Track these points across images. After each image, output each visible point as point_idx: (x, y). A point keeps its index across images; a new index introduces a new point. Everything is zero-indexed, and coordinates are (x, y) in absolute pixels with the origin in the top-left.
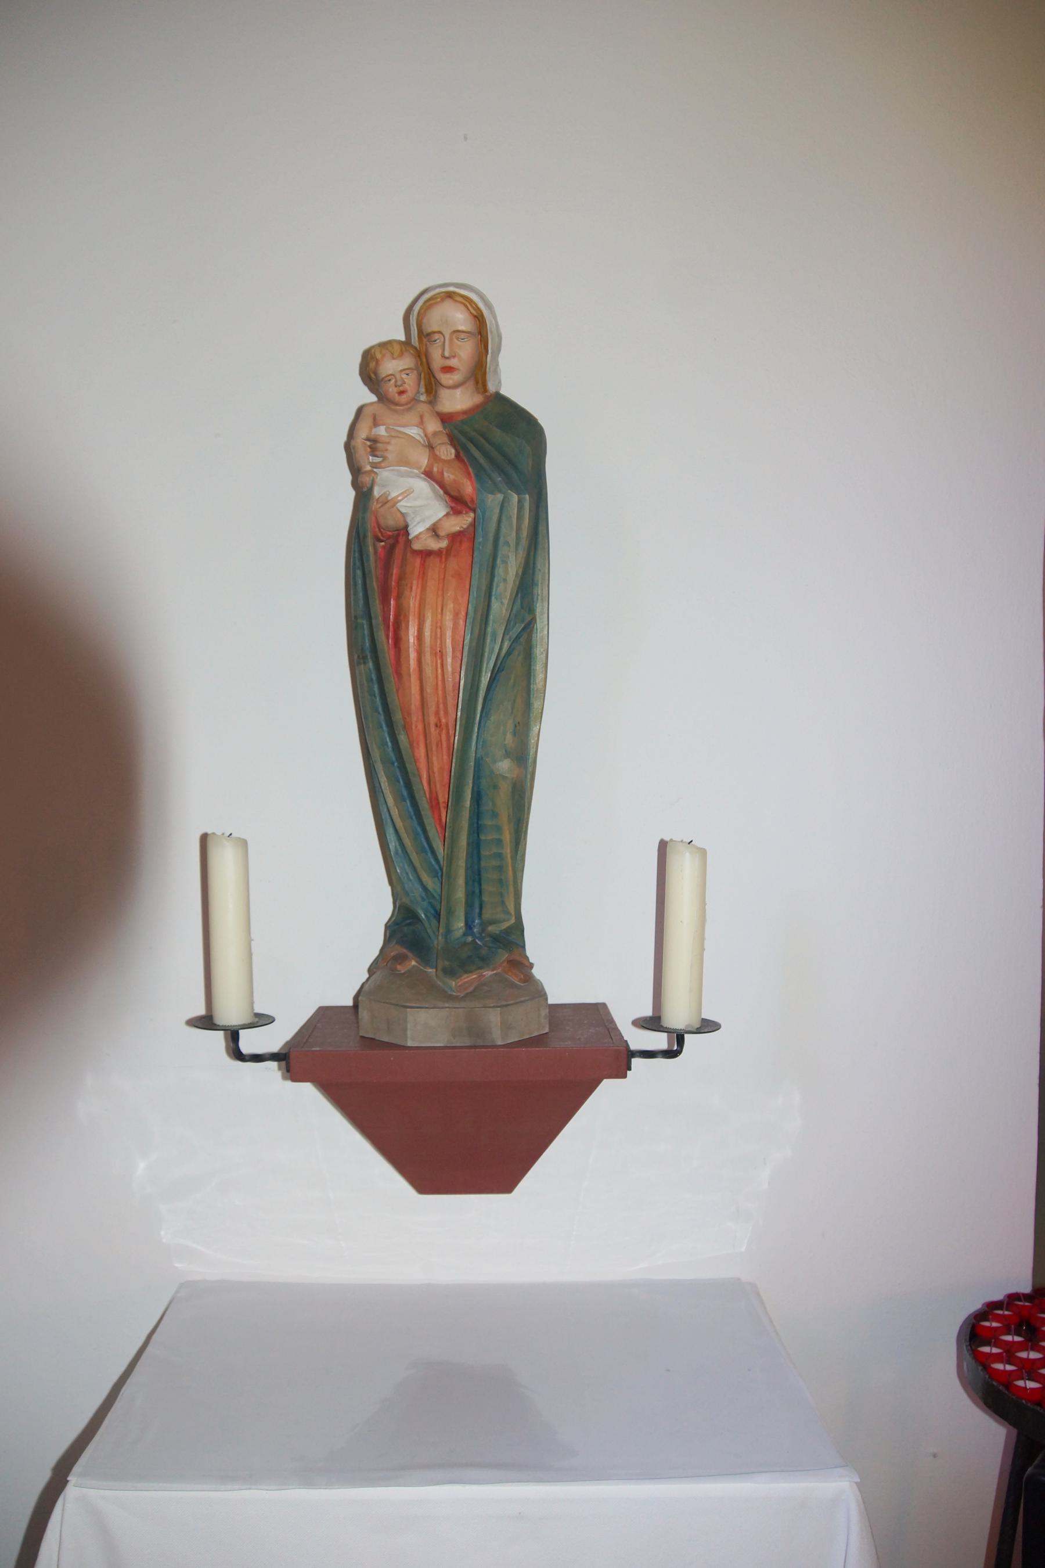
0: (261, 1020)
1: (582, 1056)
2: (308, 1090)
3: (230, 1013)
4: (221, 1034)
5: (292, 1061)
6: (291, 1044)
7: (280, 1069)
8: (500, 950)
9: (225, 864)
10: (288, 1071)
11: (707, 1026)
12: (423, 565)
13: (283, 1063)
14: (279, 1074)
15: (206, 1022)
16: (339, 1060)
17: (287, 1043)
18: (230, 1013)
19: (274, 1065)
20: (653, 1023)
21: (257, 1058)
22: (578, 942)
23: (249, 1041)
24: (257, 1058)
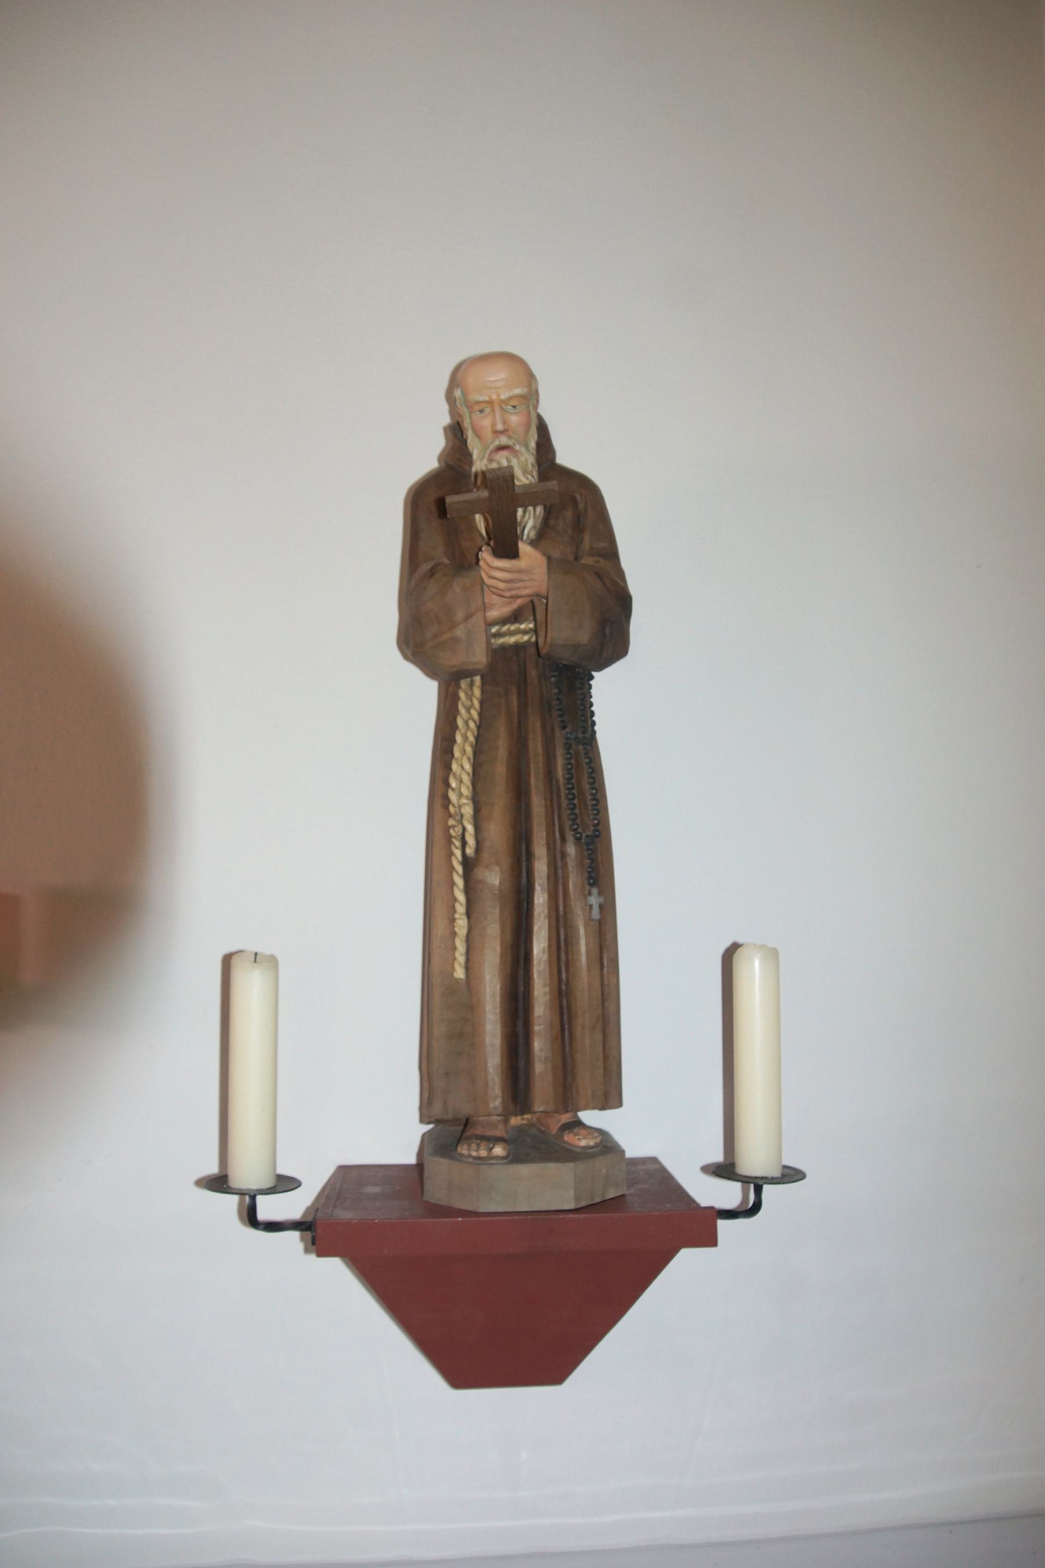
0: (285, 1184)
1: (642, 1229)
2: (335, 1270)
3: (249, 1172)
4: (235, 1199)
5: (318, 1232)
6: (314, 1209)
7: (302, 1239)
8: (497, 869)
9: (250, 987)
10: (313, 1243)
11: (791, 1175)
12: (531, 629)
13: (308, 1235)
14: (301, 1246)
15: (219, 1183)
16: (374, 1231)
17: (308, 1209)
18: (249, 1172)
19: (295, 1235)
20: (725, 1170)
21: (273, 1227)
22: (658, 1115)
23: (268, 1208)
24: (273, 1227)
